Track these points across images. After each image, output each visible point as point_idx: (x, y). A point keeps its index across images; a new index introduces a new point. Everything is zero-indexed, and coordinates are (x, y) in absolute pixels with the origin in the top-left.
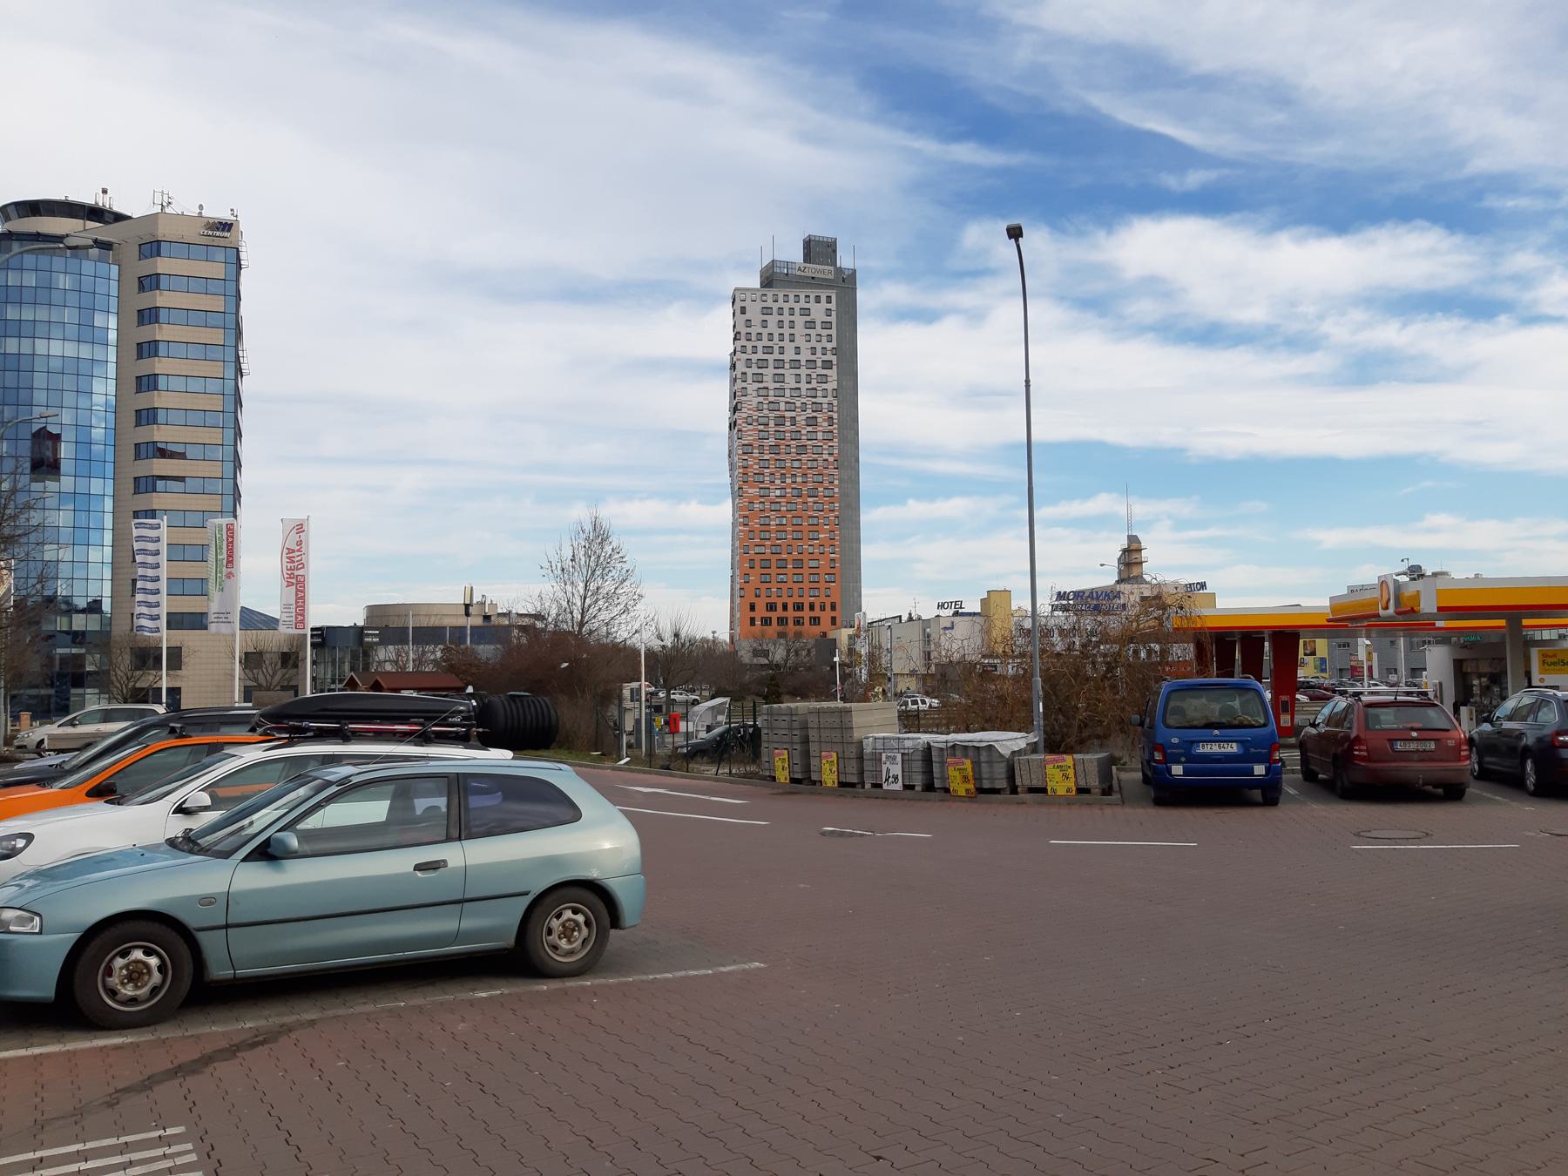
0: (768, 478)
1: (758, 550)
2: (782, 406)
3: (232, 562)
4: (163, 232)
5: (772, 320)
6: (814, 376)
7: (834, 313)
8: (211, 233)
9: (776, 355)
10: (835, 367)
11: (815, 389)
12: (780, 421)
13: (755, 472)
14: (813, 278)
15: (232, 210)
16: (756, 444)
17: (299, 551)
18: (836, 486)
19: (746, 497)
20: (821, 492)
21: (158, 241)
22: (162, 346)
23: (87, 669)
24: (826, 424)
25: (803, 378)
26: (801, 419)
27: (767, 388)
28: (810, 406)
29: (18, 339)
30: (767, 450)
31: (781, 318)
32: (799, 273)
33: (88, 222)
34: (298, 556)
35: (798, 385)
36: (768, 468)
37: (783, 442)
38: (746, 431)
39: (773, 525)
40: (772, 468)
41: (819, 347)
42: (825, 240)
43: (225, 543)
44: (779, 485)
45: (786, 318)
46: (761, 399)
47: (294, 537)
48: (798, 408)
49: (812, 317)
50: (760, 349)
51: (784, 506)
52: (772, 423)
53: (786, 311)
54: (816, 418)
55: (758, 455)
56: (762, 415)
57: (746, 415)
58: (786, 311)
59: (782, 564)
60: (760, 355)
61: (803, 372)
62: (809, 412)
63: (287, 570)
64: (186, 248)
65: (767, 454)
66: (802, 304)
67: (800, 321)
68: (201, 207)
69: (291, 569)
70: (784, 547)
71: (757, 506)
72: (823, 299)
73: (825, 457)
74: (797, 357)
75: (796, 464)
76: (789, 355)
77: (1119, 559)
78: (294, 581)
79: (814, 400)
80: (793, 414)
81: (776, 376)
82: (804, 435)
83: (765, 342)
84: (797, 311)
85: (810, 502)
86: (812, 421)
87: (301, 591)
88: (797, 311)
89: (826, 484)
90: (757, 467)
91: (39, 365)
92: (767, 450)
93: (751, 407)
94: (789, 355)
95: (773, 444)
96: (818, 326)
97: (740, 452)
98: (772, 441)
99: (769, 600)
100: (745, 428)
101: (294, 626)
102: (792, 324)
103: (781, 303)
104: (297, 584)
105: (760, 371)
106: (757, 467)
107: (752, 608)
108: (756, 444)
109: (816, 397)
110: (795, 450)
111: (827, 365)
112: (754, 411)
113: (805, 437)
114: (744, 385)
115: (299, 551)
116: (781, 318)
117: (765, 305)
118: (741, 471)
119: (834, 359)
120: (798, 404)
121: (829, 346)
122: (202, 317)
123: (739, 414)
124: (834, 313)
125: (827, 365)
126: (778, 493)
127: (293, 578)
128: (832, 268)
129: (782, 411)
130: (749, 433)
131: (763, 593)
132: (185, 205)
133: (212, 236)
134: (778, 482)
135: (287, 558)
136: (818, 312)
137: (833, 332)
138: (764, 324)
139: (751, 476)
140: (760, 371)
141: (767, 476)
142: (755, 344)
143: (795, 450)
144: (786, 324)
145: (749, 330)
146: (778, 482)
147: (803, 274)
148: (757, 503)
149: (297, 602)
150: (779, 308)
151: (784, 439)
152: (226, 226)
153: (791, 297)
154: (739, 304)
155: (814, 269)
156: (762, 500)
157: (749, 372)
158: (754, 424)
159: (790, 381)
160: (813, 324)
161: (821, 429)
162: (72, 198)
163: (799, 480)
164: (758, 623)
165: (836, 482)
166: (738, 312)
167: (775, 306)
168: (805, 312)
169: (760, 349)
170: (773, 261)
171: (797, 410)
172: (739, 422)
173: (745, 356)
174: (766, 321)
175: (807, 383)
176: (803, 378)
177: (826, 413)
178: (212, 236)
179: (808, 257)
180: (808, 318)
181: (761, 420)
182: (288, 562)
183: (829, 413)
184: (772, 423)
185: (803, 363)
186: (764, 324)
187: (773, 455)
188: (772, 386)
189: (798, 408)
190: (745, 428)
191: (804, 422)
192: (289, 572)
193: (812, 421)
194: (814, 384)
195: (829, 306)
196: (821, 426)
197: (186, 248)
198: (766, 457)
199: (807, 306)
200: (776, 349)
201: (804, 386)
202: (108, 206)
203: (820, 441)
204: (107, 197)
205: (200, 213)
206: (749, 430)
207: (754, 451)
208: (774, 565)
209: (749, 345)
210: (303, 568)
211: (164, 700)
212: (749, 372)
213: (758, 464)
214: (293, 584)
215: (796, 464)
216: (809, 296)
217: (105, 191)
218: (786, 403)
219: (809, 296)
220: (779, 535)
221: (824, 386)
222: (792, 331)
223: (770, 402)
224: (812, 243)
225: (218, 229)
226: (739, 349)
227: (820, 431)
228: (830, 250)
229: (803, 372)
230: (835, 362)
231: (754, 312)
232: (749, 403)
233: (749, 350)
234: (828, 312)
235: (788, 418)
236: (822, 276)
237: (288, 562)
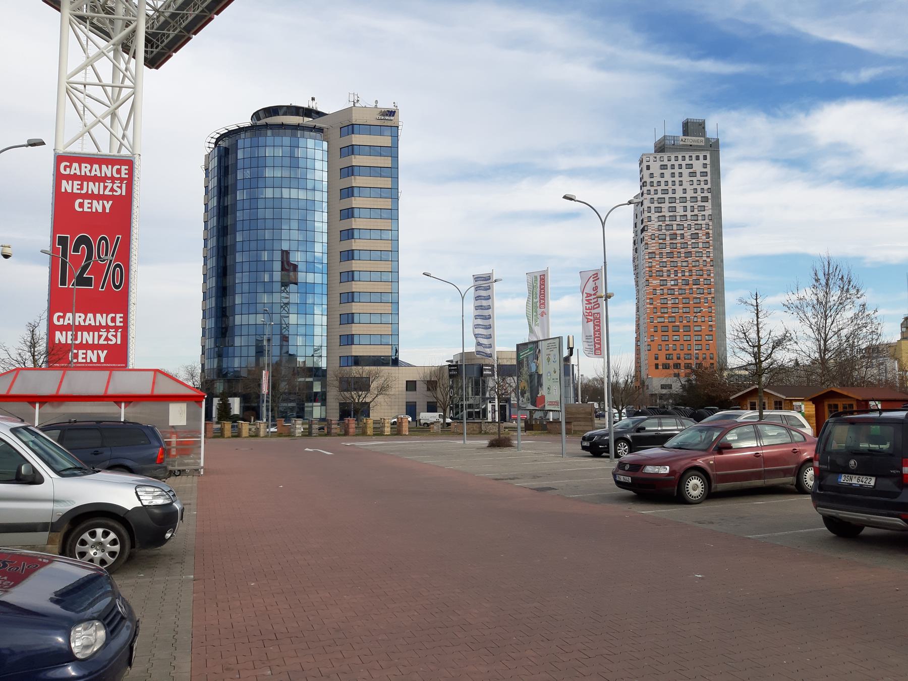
0: (666, 274)
1: (660, 320)
2: (675, 227)
3: (544, 304)
4: (356, 118)
5: (668, 173)
6: (696, 207)
7: (708, 166)
8: (383, 118)
9: (670, 195)
10: (710, 201)
11: (697, 215)
12: (674, 236)
13: (657, 269)
14: (691, 145)
15: (394, 103)
16: (657, 252)
17: (594, 294)
18: (712, 277)
19: (651, 286)
20: (702, 281)
21: (352, 124)
22: (356, 190)
23: (314, 391)
24: (704, 237)
25: (689, 209)
26: (688, 235)
27: (665, 216)
28: (694, 226)
29: (272, 189)
30: (664, 255)
31: (673, 171)
32: (682, 143)
33: (305, 118)
34: (594, 299)
35: (685, 213)
36: (666, 267)
37: (676, 250)
38: (651, 244)
39: (669, 304)
40: (668, 267)
41: (699, 188)
42: (698, 121)
43: (539, 289)
44: (673, 278)
45: (677, 171)
46: (660, 223)
47: (591, 284)
48: (686, 227)
49: (694, 169)
50: (659, 192)
51: (677, 291)
52: (668, 238)
53: (677, 167)
54: (698, 233)
55: (659, 259)
56: (661, 233)
57: (650, 234)
58: (677, 167)
59: (676, 329)
60: (660, 195)
61: (689, 204)
62: (693, 231)
63: (586, 309)
64: (369, 129)
65: (664, 258)
66: (687, 161)
67: (686, 172)
68: (376, 102)
69: (589, 309)
70: (677, 318)
71: (659, 291)
72: (701, 157)
73: (705, 258)
74: (684, 195)
75: (685, 264)
76: (679, 194)
77: (902, 324)
78: (591, 318)
79: (696, 222)
80: (682, 232)
81: (671, 208)
82: (690, 245)
83: (663, 187)
84: (684, 166)
85: (695, 288)
86: (695, 236)
87: (597, 325)
88: (684, 166)
89: (705, 276)
90: (659, 266)
91: (285, 204)
92: (664, 255)
93: (654, 228)
94: (679, 194)
95: (669, 251)
96: (698, 174)
97: (647, 257)
98: (668, 250)
99: (668, 352)
100: (650, 242)
101: (593, 352)
102: (681, 175)
103: (673, 162)
104: (594, 320)
105: (660, 205)
106: (659, 266)
107: (657, 358)
108: (657, 252)
109: (697, 220)
110: (684, 255)
111: (705, 199)
112: (657, 231)
113: (691, 247)
114: (649, 214)
115: (594, 294)
116: (673, 171)
117: (662, 163)
118: (648, 269)
119: (709, 195)
120: (686, 225)
121: (706, 187)
122: (373, 171)
123: (646, 233)
124: (708, 166)
125: (705, 199)
126: (673, 283)
127: (591, 316)
128: (703, 139)
129: (675, 230)
130: (653, 245)
131: (664, 348)
132: (367, 101)
133: (384, 119)
134: (672, 276)
135: (586, 300)
136: (698, 166)
137: (708, 178)
138: (662, 175)
139: (654, 273)
140: (660, 205)
141: (665, 272)
142: (656, 188)
143: (684, 255)
144: (677, 175)
145: (652, 180)
146: (672, 276)
147: (684, 143)
148: (658, 290)
149: (595, 334)
150: (672, 165)
151: (676, 248)
152: (392, 113)
153: (680, 158)
154: (645, 164)
155: (690, 140)
156: (662, 288)
157: (653, 206)
158: (656, 239)
159: (680, 211)
160: (694, 174)
161: (701, 240)
162: (293, 105)
163: (687, 274)
164: (660, 367)
165: (712, 275)
166: (645, 168)
167: (669, 164)
168: (690, 166)
169: (659, 192)
170: (665, 136)
171: (685, 229)
172: (646, 238)
173: (650, 196)
174: (674, 173)
175: (691, 211)
176: (689, 209)
177: (704, 230)
178: (384, 119)
179: (686, 132)
180: (691, 170)
181: (661, 237)
182: (586, 304)
183: (706, 230)
184: (668, 238)
185: (688, 199)
186: (662, 175)
187: (669, 259)
188: (668, 214)
189: (686, 227)
190: (650, 242)
191: (689, 237)
192: (588, 311)
193: (695, 236)
194: (696, 212)
195: (705, 162)
196: (702, 239)
197: (369, 129)
198: (664, 260)
199: (690, 162)
200: (670, 191)
201: (689, 213)
202: (311, 107)
203: (700, 248)
204: (314, 102)
205: (376, 106)
206: (653, 243)
207: (656, 256)
208: (670, 329)
209: (652, 189)
210: (599, 307)
211: (505, 404)
212: (653, 206)
213: (659, 264)
214: (591, 320)
215: (685, 264)
216: (691, 156)
217: (313, 99)
218: (677, 225)
219: (691, 156)
220: (674, 310)
221: (703, 213)
222: (681, 179)
223: (667, 225)
224: (689, 124)
225: (387, 115)
226: (645, 192)
227: (701, 242)
228: (701, 127)
229: (689, 204)
230: (710, 197)
231: (655, 168)
232: (652, 226)
233: (652, 192)
234: (705, 166)
235: (678, 234)
236: (695, 144)
237: (586, 304)
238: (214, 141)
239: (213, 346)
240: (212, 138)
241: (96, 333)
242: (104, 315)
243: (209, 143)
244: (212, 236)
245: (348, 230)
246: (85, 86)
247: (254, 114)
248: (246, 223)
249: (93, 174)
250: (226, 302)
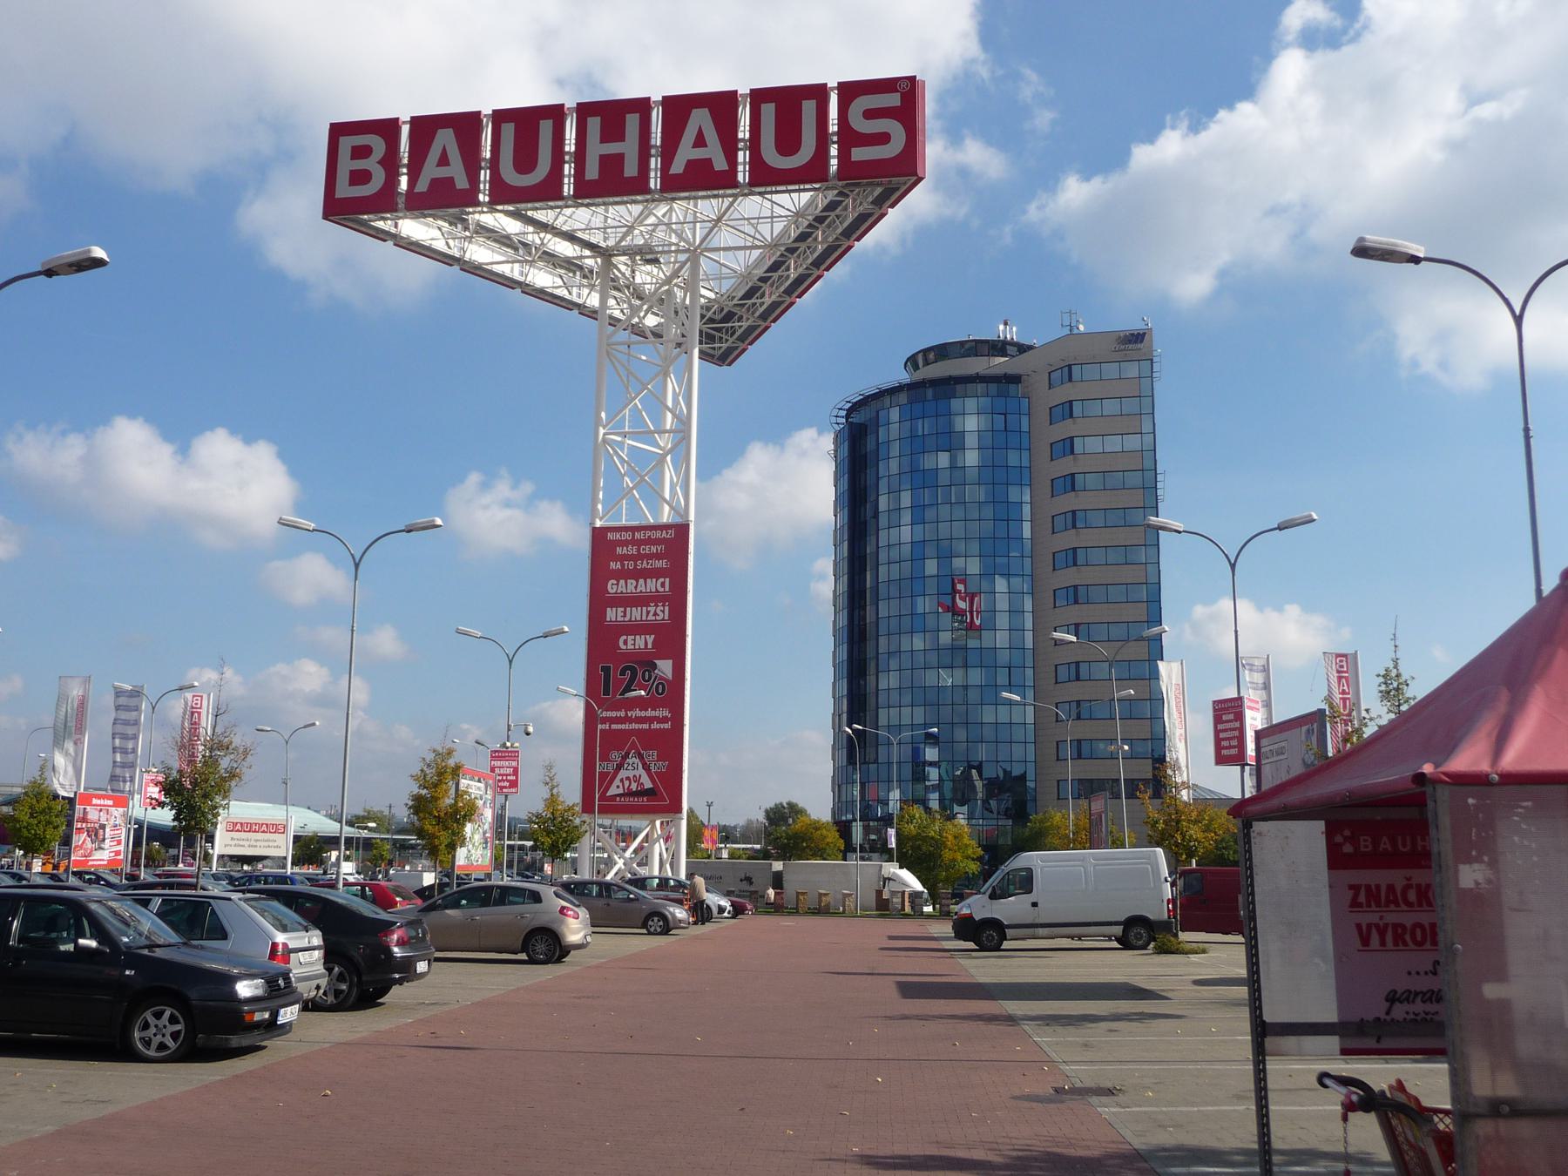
238: (843, 413)
239: (845, 764)
240: (841, 409)
241: (644, 609)
242: (654, 580)
243: (837, 416)
244: (842, 441)
245: (1067, 587)
246: (629, 347)
247: (908, 360)
248: (894, 622)
249: (638, 591)
250: (865, 717)
